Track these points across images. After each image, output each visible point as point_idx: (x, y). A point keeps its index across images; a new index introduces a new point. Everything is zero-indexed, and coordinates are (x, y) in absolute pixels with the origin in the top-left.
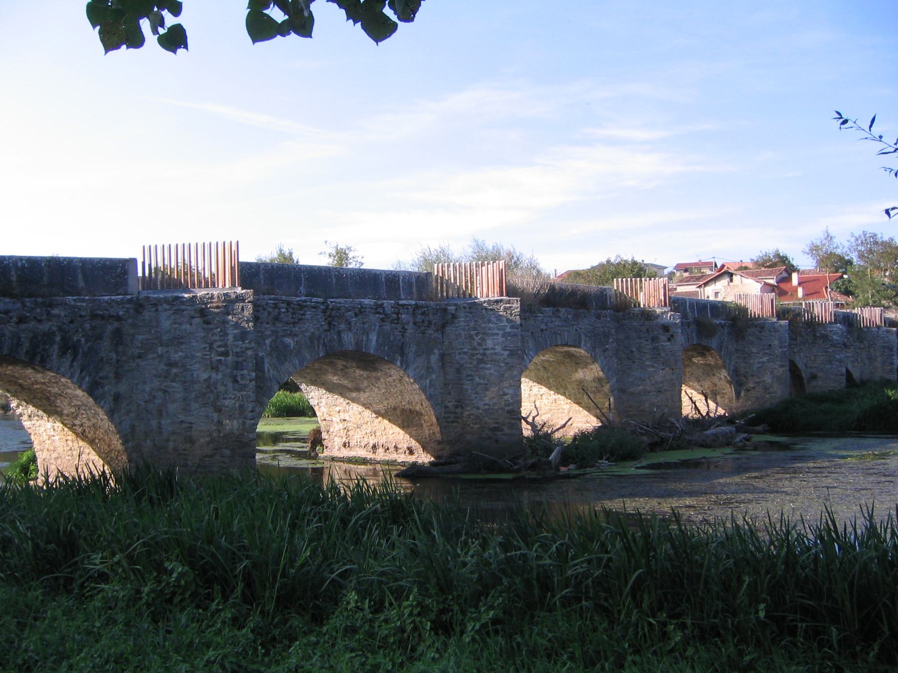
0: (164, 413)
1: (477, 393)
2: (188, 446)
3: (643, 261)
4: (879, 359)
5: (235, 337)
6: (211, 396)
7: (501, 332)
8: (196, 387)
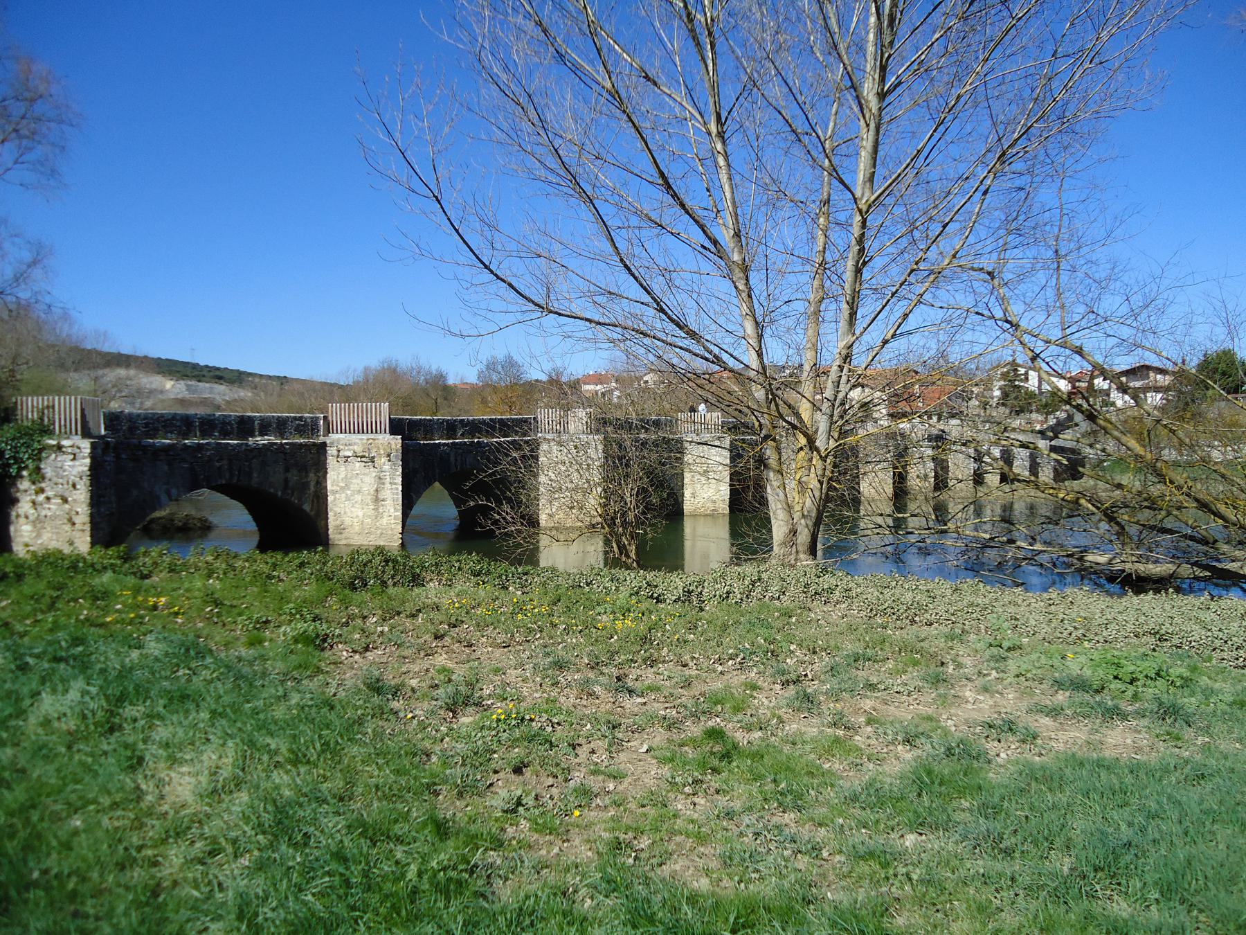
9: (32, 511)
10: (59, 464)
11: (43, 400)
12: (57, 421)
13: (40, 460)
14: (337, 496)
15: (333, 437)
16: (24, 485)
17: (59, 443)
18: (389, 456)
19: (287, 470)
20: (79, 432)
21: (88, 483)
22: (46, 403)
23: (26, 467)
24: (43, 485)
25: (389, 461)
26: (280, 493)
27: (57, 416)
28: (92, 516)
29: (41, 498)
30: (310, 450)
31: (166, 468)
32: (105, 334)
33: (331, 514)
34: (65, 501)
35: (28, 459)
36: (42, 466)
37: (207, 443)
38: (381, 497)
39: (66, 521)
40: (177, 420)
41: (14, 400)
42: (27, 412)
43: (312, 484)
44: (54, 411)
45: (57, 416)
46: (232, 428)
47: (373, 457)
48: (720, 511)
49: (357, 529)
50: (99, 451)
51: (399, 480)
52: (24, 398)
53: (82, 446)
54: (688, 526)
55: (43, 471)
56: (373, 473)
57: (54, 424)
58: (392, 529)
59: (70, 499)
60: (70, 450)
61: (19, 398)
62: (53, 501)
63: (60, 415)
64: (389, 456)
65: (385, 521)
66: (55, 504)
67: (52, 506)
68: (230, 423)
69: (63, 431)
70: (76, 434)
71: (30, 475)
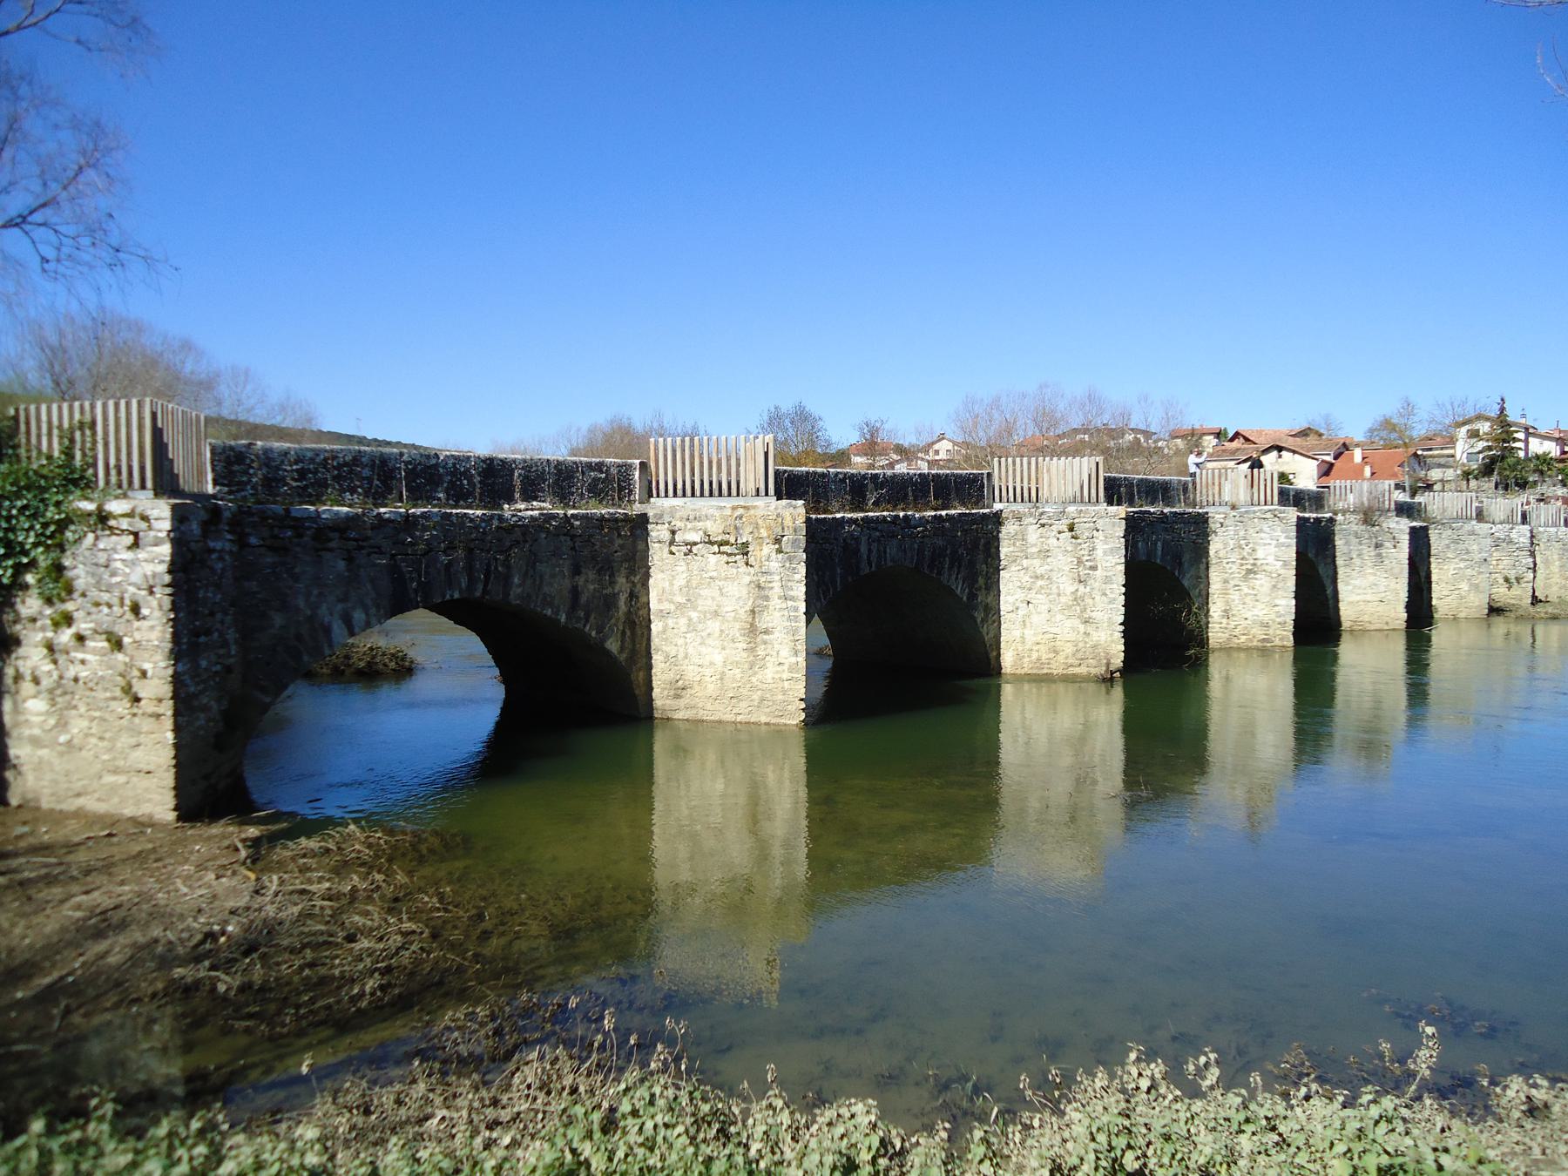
0: (1028, 624)
1: (1244, 604)
2: (1052, 655)
4: (1557, 563)
5: (1105, 553)
6: (1078, 608)
7: (1274, 542)
8: (1063, 599)
9: (47, 667)
10: (102, 558)
11: (71, 408)
12: (101, 456)
13: (62, 548)
14: (670, 622)
15: (658, 506)
16: (30, 605)
17: (100, 509)
18: (778, 541)
19: (576, 571)
20: (149, 484)
21: (167, 602)
22: (77, 416)
23: (33, 564)
24: (69, 606)
25: (779, 551)
26: (563, 618)
27: (100, 447)
28: (177, 680)
29: (65, 636)
30: (618, 529)
31: (341, 565)
32: (247, 371)
33: (657, 659)
34: (117, 645)
35: (36, 545)
36: (67, 562)
37: (423, 515)
38: (762, 625)
39: (118, 693)
40: (364, 466)
41: (12, 412)
42: (39, 436)
43: (623, 598)
44: (94, 434)
45: (100, 447)
46: (471, 483)
47: (745, 545)
48: (1277, 642)
49: (711, 688)
50: (195, 527)
51: (800, 590)
52: (32, 408)
53: (153, 513)
54: (1216, 668)
55: (69, 574)
56: (745, 576)
57: (95, 465)
58: (784, 692)
59: (126, 640)
60: (124, 524)
61: (22, 407)
62: (90, 644)
63: (106, 445)
64: (778, 541)
65: (769, 673)
66: (94, 651)
67: (88, 657)
68: (467, 472)
69: (113, 479)
70: (143, 487)
71: (39, 581)
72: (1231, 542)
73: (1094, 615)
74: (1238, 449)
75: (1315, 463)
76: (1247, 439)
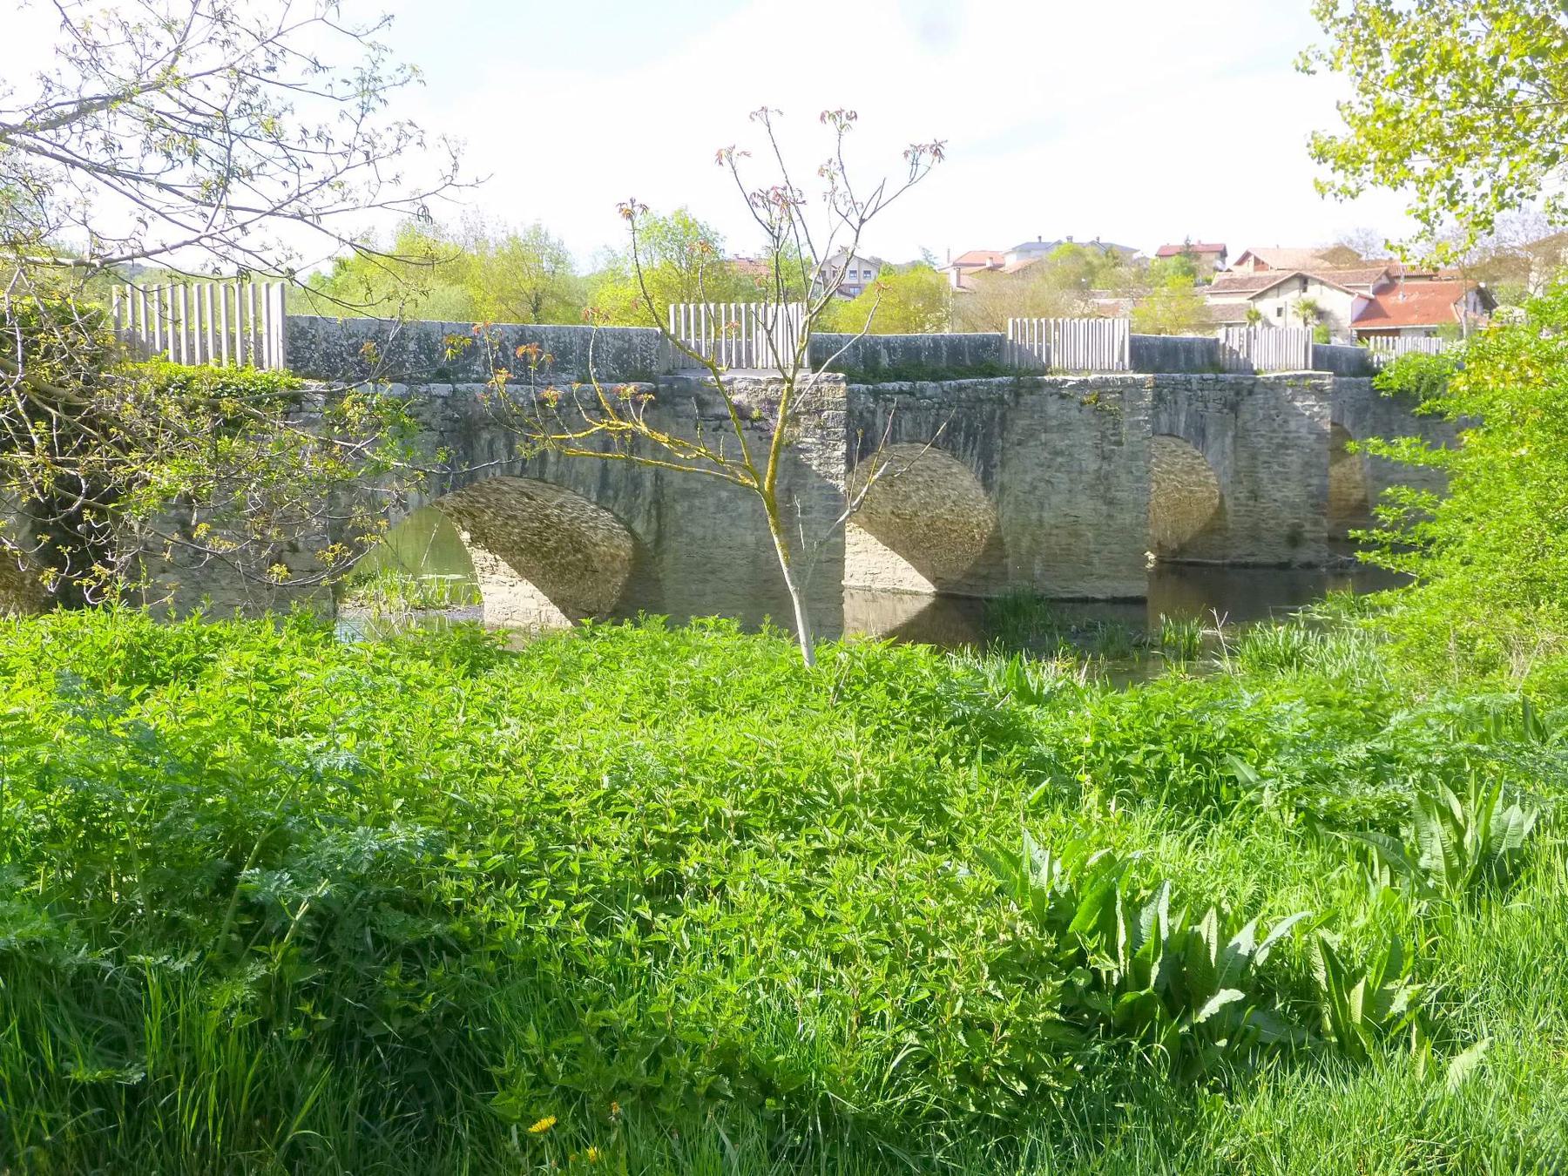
3: (1069, 239)
8: (1085, 478)
72: (1261, 412)
73: (1119, 495)
74: (1250, 279)
75: (1350, 299)
76: (1257, 261)
